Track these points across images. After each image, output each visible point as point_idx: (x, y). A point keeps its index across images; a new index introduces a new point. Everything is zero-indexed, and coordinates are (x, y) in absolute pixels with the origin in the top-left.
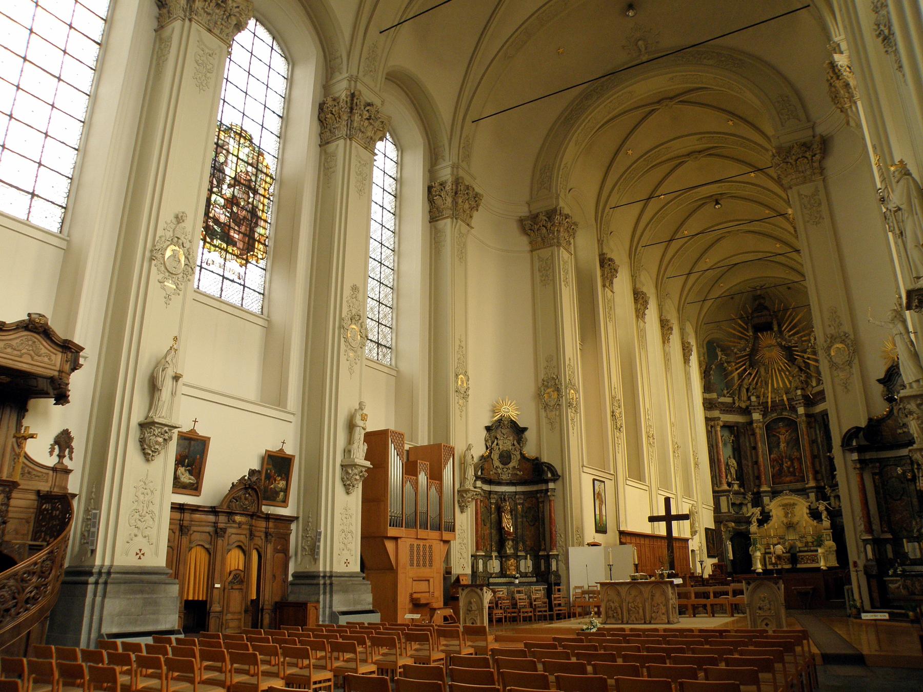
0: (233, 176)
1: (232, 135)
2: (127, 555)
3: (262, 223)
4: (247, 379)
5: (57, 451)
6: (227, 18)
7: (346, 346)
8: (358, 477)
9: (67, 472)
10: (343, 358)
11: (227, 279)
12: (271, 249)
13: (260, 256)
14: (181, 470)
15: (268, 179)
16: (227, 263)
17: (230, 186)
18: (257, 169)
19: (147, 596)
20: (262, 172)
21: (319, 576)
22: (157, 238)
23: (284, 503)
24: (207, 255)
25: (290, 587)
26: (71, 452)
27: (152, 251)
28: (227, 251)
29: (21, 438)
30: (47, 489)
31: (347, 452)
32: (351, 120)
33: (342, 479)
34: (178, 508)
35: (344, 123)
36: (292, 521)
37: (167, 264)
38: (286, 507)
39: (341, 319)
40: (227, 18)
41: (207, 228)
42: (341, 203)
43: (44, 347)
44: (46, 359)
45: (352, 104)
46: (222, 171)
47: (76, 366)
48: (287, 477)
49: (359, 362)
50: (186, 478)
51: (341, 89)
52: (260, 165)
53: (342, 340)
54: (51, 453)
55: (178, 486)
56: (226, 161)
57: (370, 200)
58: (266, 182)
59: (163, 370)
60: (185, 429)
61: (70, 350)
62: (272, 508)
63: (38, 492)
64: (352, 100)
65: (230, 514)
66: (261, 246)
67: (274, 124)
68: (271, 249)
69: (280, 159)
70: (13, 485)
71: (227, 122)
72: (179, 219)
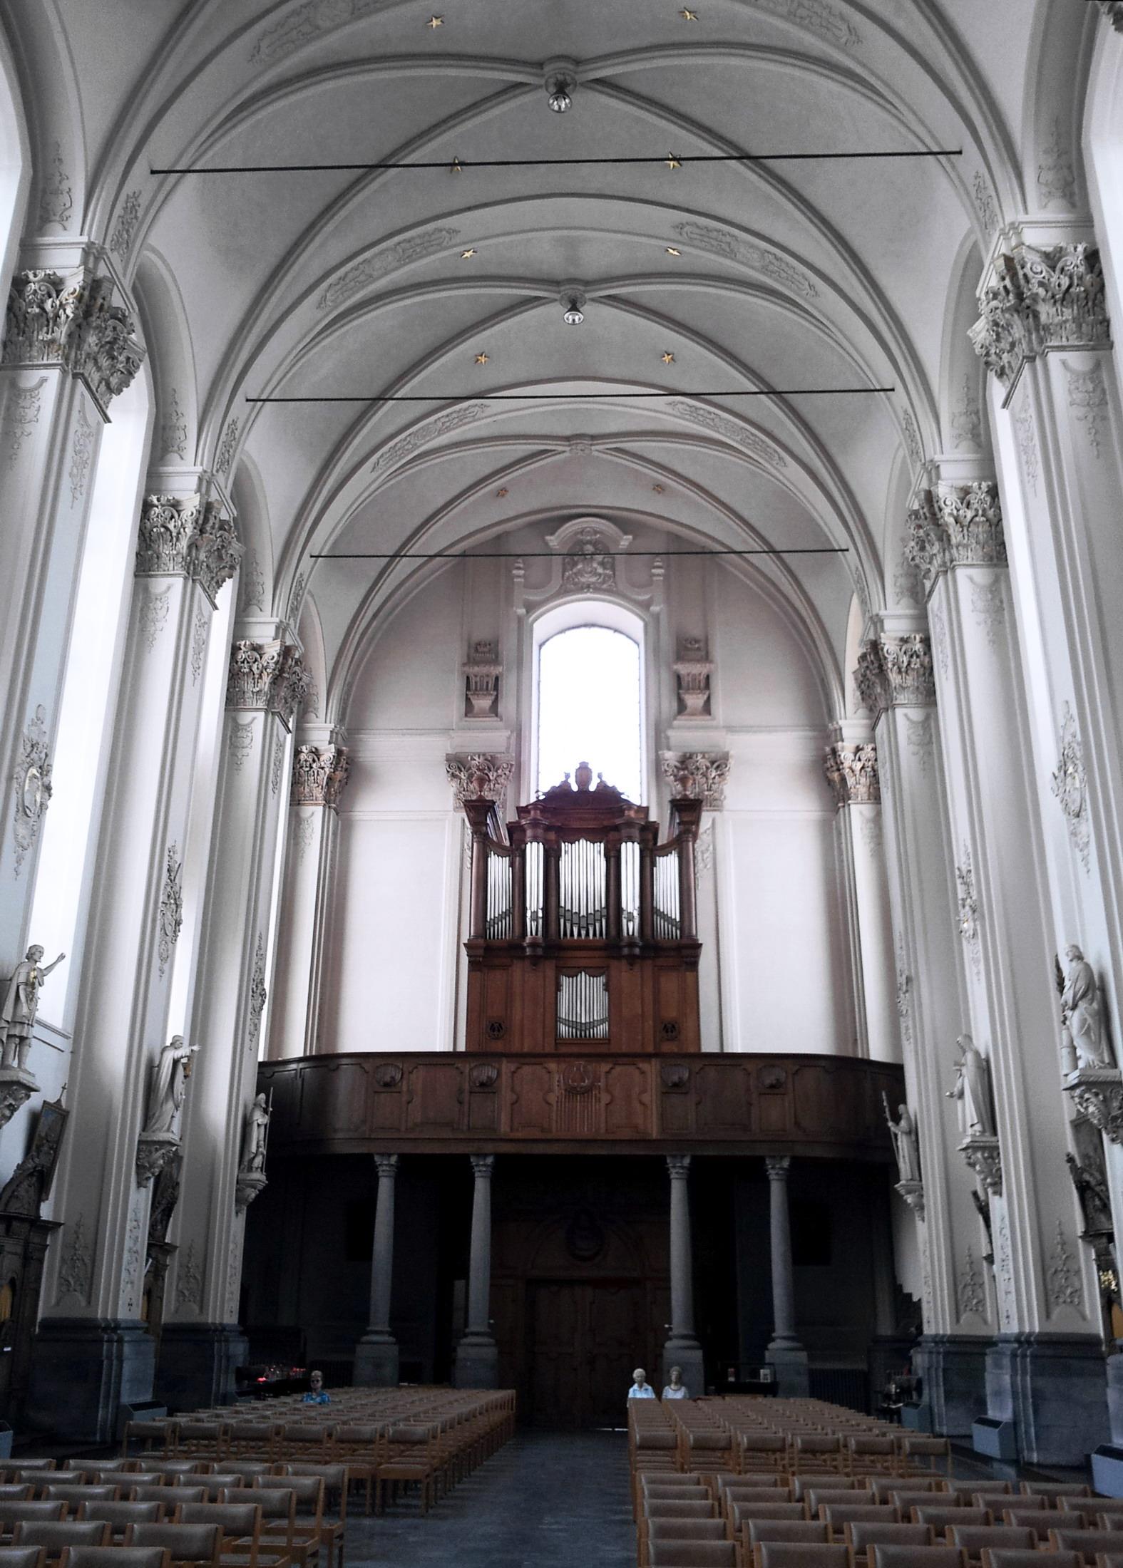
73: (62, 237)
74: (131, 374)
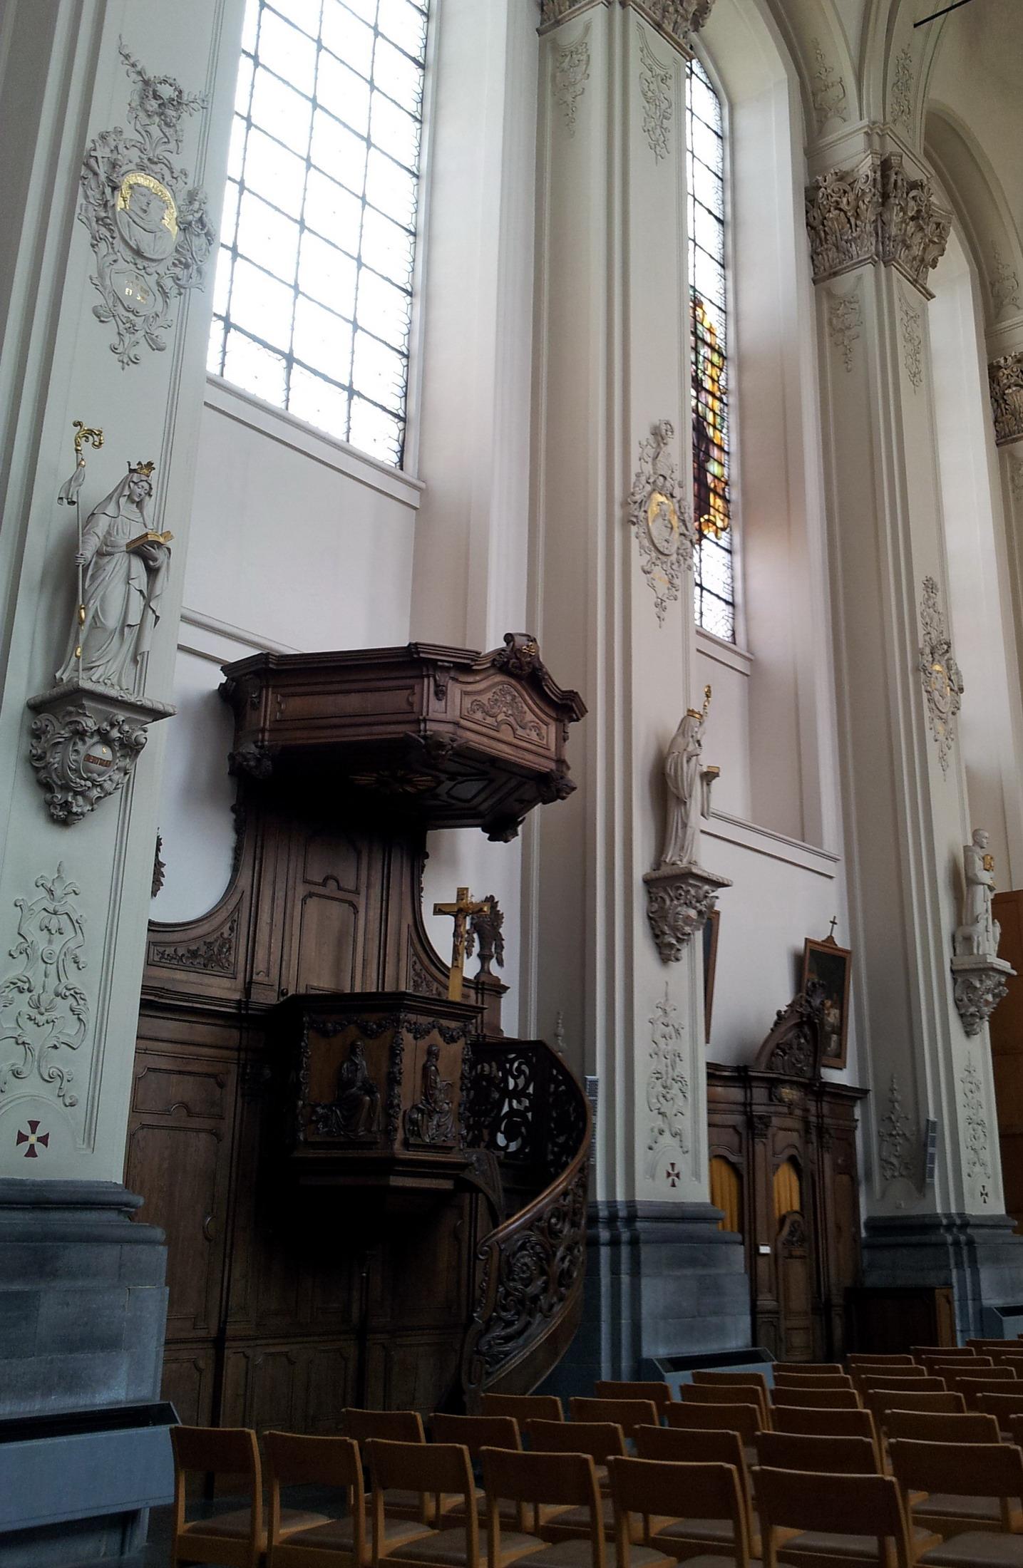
2: (653, 1177)
3: (715, 453)
8: (990, 998)
13: (720, 524)
15: (716, 358)
19: (704, 1272)
21: (939, 1225)
22: (633, 478)
25: (865, 1253)
27: (625, 504)
31: (962, 940)
32: (881, 223)
33: (958, 1002)
35: (869, 228)
36: (855, 1099)
44: (534, 736)
45: (884, 185)
49: (952, 744)
51: (853, 153)
52: (699, 327)
65: (772, 1084)
66: (719, 503)
73: (847, 128)
74: (942, 238)
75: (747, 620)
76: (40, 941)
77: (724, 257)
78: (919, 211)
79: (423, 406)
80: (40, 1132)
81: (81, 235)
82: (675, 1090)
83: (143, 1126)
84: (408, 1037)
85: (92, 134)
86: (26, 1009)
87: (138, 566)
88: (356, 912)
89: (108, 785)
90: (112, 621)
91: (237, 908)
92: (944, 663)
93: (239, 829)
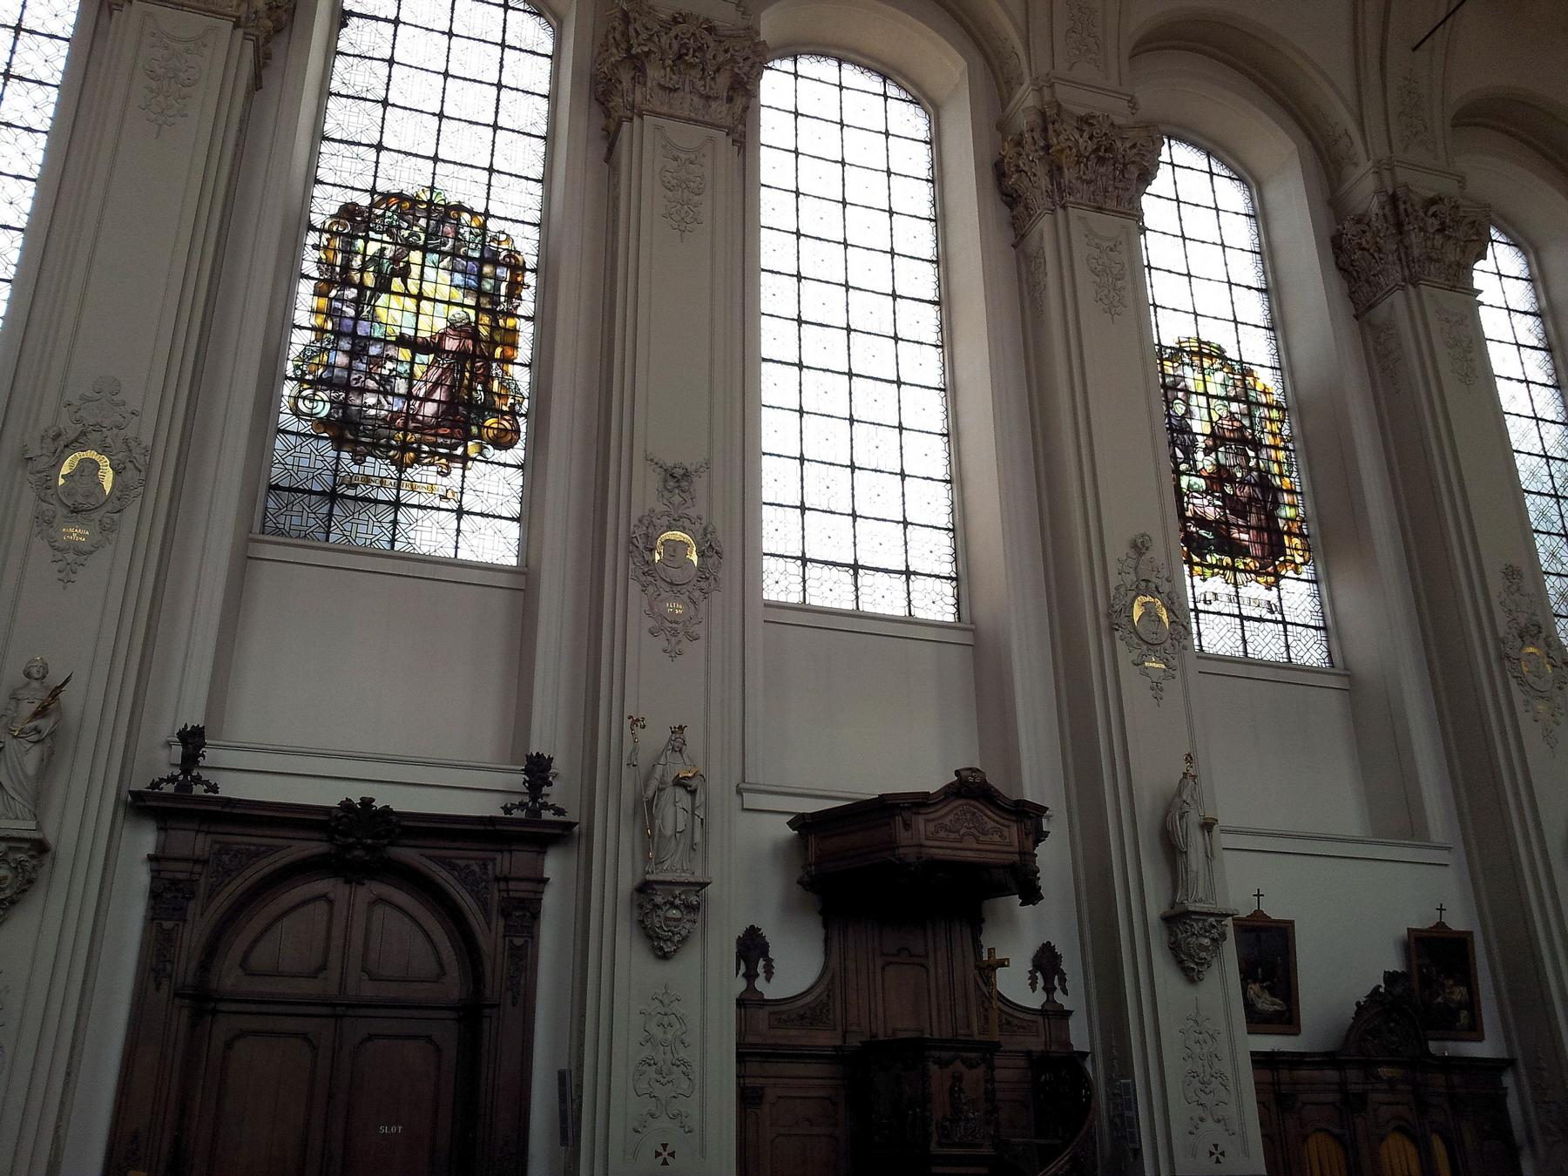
0: (1208, 431)
1: (1187, 360)
3: (1287, 498)
4: (1337, 801)
5: (1040, 982)
6: (1122, 172)
7: (1526, 693)
9: (1066, 1014)
10: (1525, 720)
11: (1250, 618)
12: (1315, 541)
13: (1299, 560)
14: (1254, 988)
15: (1274, 414)
16: (1242, 591)
17: (1207, 451)
18: (1248, 402)
20: (1259, 405)
23: (1474, 1031)
24: (1201, 587)
26: (1063, 980)
27: (1109, 615)
28: (1235, 570)
29: (988, 969)
30: (1041, 1048)
34: (1262, 1061)
37: (1141, 630)
38: (1480, 1038)
39: (1500, 642)
40: (1122, 172)
41: (1188, 539)
42: (1427, 384)
43: (989, 819)
45: (1397, 215)
46: (1187, 430)
47: (1040, 836)
48: (1466, 976)
50: (1267, 1003)
51: (1365, 191)
52: (1252, 393)
53: (1513, 683)
54: (1033, 986)
55: (1257, 1021)
56: (1188, 412)
57: (1489, 378)
58: (1271, 421)
59: (1181, 818)
60: (1244, 913)
61: (1029, 816)
62: (1450, 1044)
63: (1029, 1053)
64: (1395, 208)
66: (1296, 541)
67: (1254, 308)
68: (1315, 541)
69: (1285, 366)
70: (992, 1048)
71: (1169, 340)
72: (1139, 547)
75: (1339, 638)
76: (658, 1033)
77: (1272, 320)
78: (1443, 223)
79: (967, 567)
80: (669, 1150)
81: (634, 587)
82: (1215, 1083)
83: (779, 1135)
84: (934, 1068)
85: (634, 521)
86: (654, 1076)
87: (680, 792)
88: (928, 972)
89: (684, 933)
90: (669, 832)
91: (832, 980)
92: (1541, 642)
93: (826, 925)
